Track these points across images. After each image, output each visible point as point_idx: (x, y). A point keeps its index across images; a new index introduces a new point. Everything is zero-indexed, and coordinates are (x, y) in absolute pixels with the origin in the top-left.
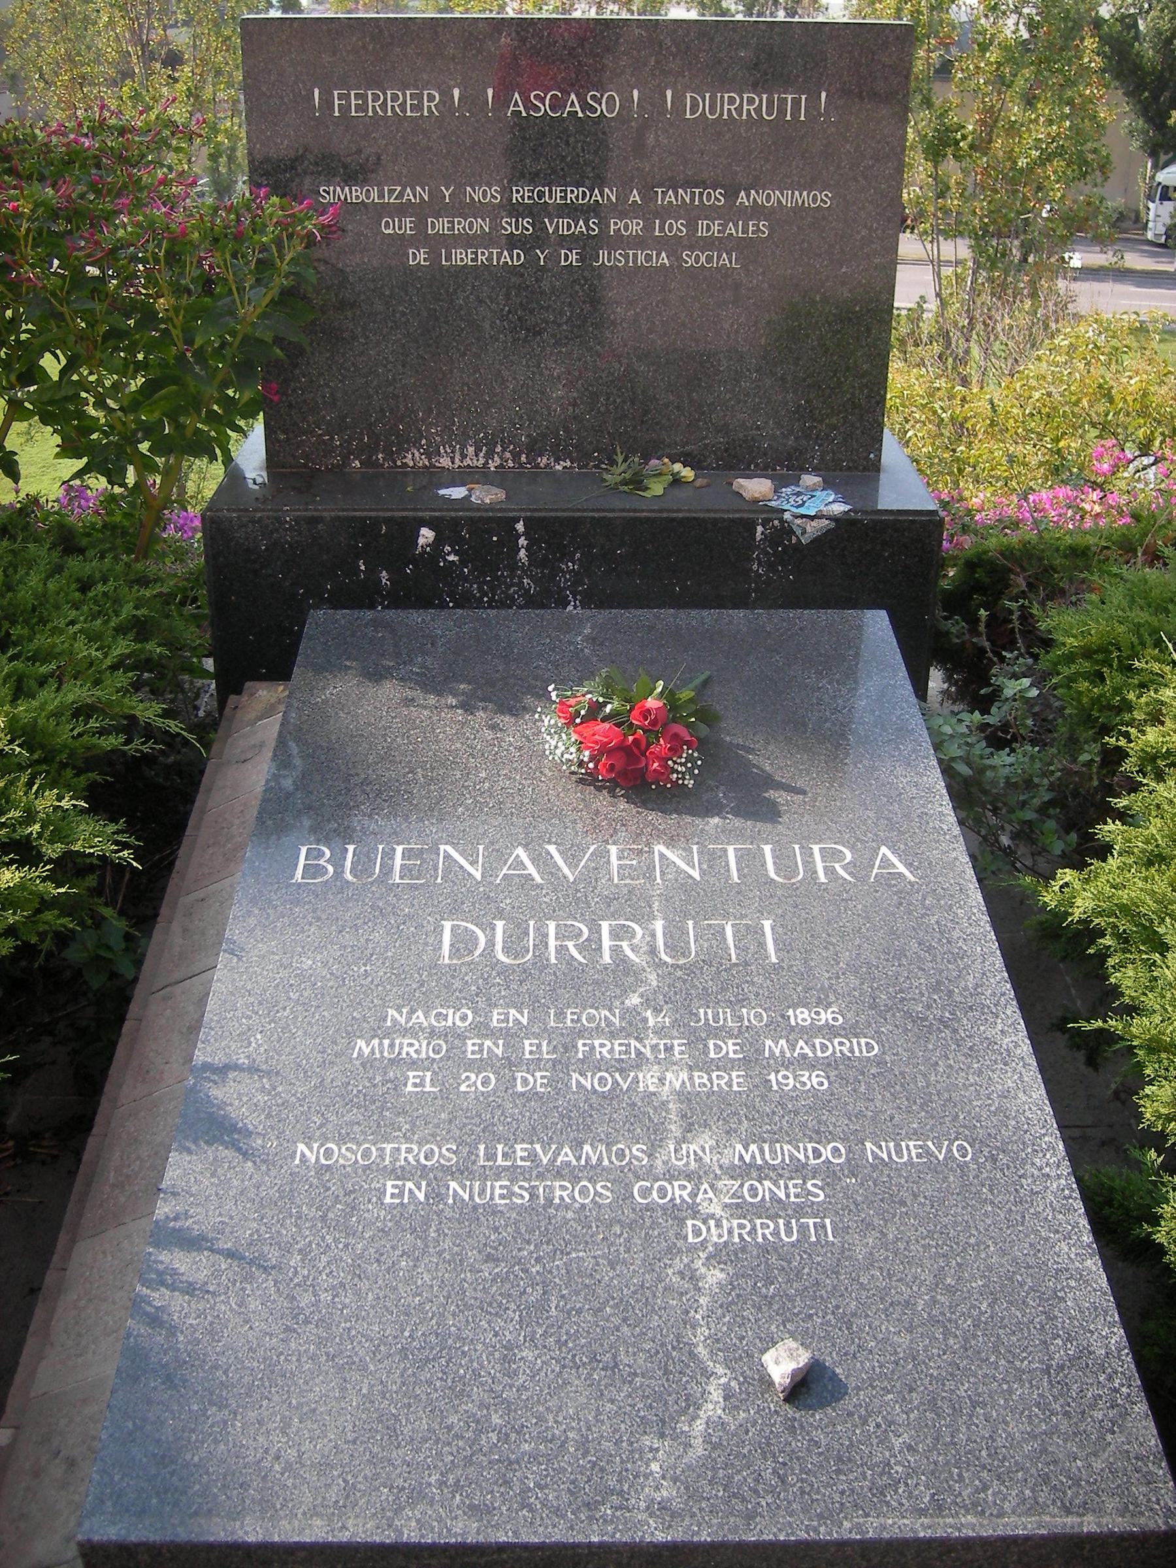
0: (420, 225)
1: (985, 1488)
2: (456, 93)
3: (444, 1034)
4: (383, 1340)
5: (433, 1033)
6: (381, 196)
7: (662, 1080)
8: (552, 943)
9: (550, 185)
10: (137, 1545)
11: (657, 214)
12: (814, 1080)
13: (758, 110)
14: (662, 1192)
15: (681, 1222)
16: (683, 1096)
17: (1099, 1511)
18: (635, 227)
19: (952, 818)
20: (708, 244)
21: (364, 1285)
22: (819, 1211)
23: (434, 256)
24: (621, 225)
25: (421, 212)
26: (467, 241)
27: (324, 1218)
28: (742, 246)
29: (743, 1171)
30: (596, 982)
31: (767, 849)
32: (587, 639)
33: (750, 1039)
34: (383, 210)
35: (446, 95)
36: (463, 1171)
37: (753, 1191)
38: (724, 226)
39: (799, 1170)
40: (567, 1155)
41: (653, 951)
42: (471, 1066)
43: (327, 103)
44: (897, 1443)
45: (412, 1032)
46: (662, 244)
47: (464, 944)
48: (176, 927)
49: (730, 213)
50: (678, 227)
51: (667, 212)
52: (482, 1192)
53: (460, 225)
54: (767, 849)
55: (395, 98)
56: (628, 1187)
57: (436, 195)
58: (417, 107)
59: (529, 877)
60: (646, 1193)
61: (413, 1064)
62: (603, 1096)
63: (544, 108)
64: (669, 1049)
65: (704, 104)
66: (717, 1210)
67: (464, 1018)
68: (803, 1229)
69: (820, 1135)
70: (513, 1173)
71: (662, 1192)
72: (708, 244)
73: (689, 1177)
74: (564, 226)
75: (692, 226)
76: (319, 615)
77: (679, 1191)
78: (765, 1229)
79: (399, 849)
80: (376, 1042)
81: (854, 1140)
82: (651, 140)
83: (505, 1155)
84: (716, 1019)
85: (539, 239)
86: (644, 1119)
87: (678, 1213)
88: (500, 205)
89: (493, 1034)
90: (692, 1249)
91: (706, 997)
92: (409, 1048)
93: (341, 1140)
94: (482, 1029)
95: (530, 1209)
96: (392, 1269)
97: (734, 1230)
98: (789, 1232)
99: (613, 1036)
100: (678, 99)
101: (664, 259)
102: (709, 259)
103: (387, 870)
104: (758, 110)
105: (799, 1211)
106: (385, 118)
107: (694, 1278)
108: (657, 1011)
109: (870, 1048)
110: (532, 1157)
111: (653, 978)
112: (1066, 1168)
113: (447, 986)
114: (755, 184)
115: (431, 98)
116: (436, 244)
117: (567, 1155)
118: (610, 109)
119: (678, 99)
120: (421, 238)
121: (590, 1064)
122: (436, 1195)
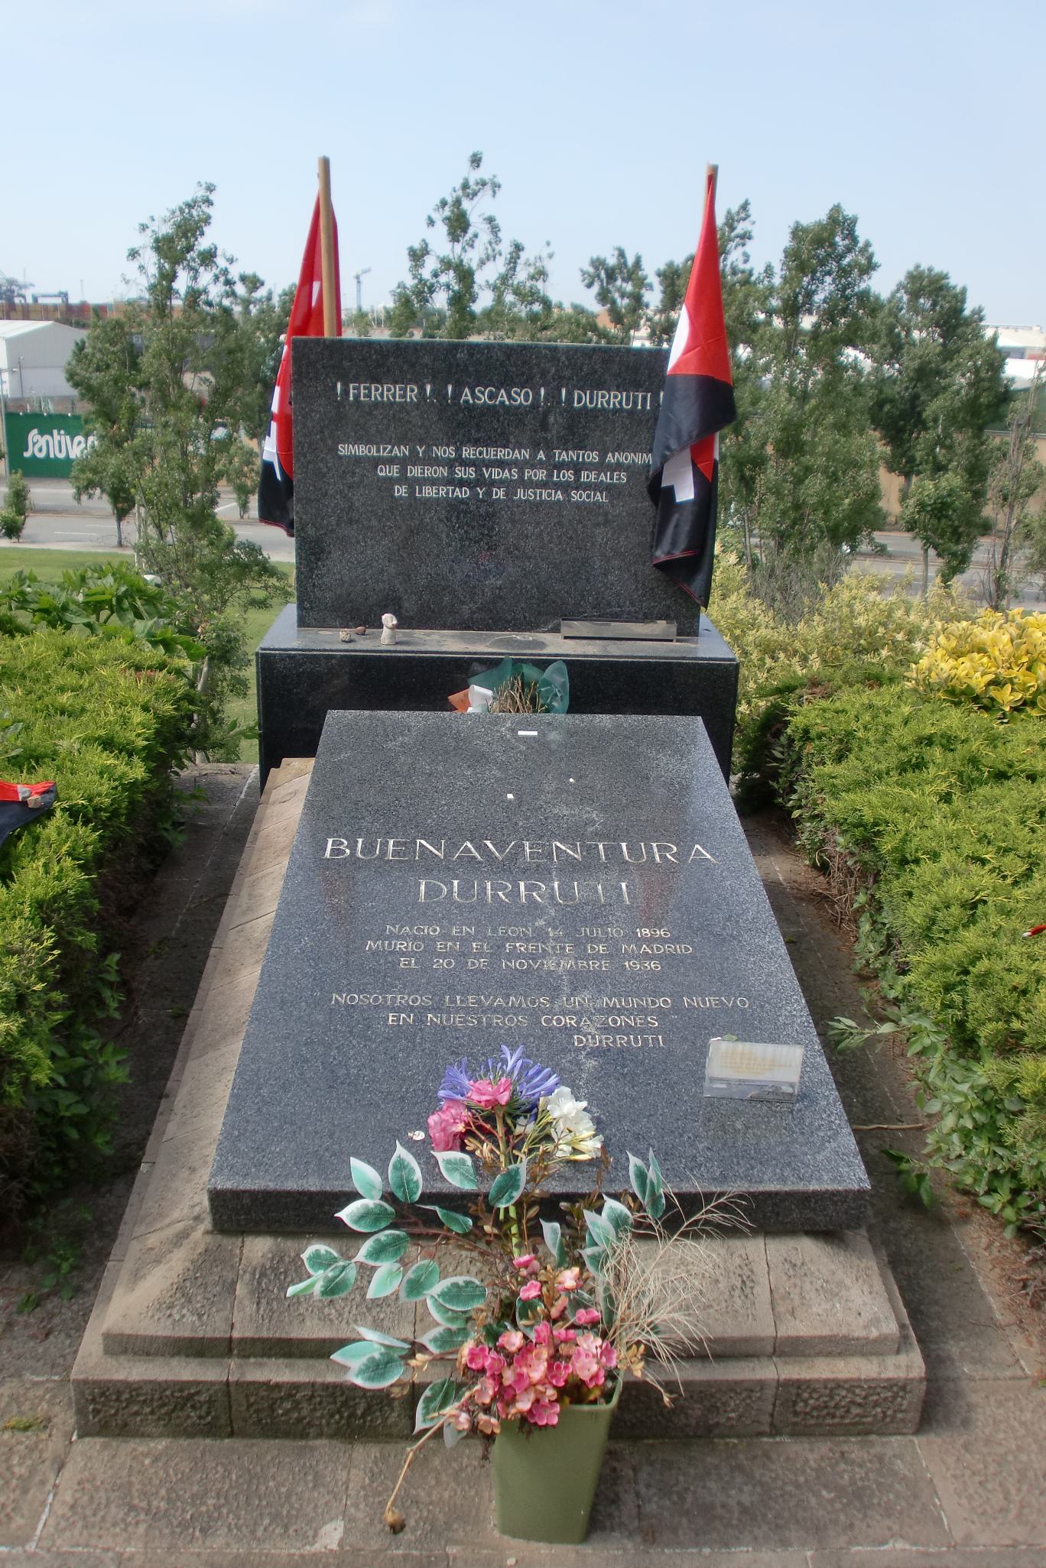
0: (403, 471)
1: (753, 1168)
2: (428, 388)
3: (423, 939)
4: (389, 1093)
5: (415, 938)
6: (378, 451)
7: (558, 964)
8: (489, 892)
9: (487, 446)
10: (244, 1192)
11: (555, 467)
12: (600, 498)
13: (620, 403)
14: (559, 1021)
15: (571, 1037)
16: (569, 972)
17: (819, 1180)
18: (541, 475)
19: (740, 829)
20: (588, 487)
21: (377, 1065)
22: (655, 1032)
23: (411, 491)
24: (532, 473)
25: (404, 463)
26: (433, 482)
27: (351, 1032)
28: (609, 488)
29: (610, 1011)
30: (516, 913)
31: (624, 845)
32: (508, 729)
33: (613, 944)
34: (376, 462)
35: (422, 389)
36: (436, 1009)
37: (615, 1021)
38: (598, 475)
39: (643, 1011)
40: (499, 1001)
41: (552, 897)
42: (439, 955)
43: (346, 392)
44: (701, 1146)
45: (403, 938)
46: (558, 486)
47: (433, 891)
48: (244, 892)
49: (601, 467)
50: (568, 475)
51: (561, 466)
52: (448, 1020)
53: (429, 472)
54: (624, 845)
55: (389, 390)
56: (538, 1019)
57: (413, 451)
58: (404, 396)
59: (474, 858)
60: (548, 1021)
61: (403, 954)
62: (522, 972)
63: (484, 399)
64: (563, 948)
65: (586, 399)
66: (593, 1031)
67: (435, 931)
68: (645, 1041)
69: (655, 993)
70: (468, 1010)
71: (559, 1021)
72: (588, 487)
73: (575, 1014)
74: (496, 474)
75: (577, 474)
76: (333, 716)
77: (570, 1021)
78: (622, 1040)
79: (391, 842)
80: (380, 943)
81: (677, 997)
82: (551, 420)
83: (462, 1001)
84: (592, 932)
85: (480, 481)
86: (550, 986)
87: (568, 1031)
88: (455, 459)
89: (454, 939)
90: (578, 1050)
91: (585, 922)
92: (401, 945)
93: (361, 992)
94: (446, 936)
95: (478, 1028)
96: (394, 1058)
97: (600, 1040)
98: (636, 1041)
99: (528, 941)
100: (570, 394)
101: (560, 496)
102: (588, 496)
103: (384, 852)
104: (620, 403)
105: (642, 1031)
106: (382, 402)
107: (578, 1064)
108: (555, 928)
109: (687, 949)
110: (479, 1002)
111: (552, 912)
112: (806, 1012)
113: (425, 914)
114: (619, 448)
115: (412, 390)
116: (413, 483)
117: (499, 1001)
118: (526, 400)
119: (570, 394)
120: (403, 479)
121: (514, 955)
122: (420, 1020)
